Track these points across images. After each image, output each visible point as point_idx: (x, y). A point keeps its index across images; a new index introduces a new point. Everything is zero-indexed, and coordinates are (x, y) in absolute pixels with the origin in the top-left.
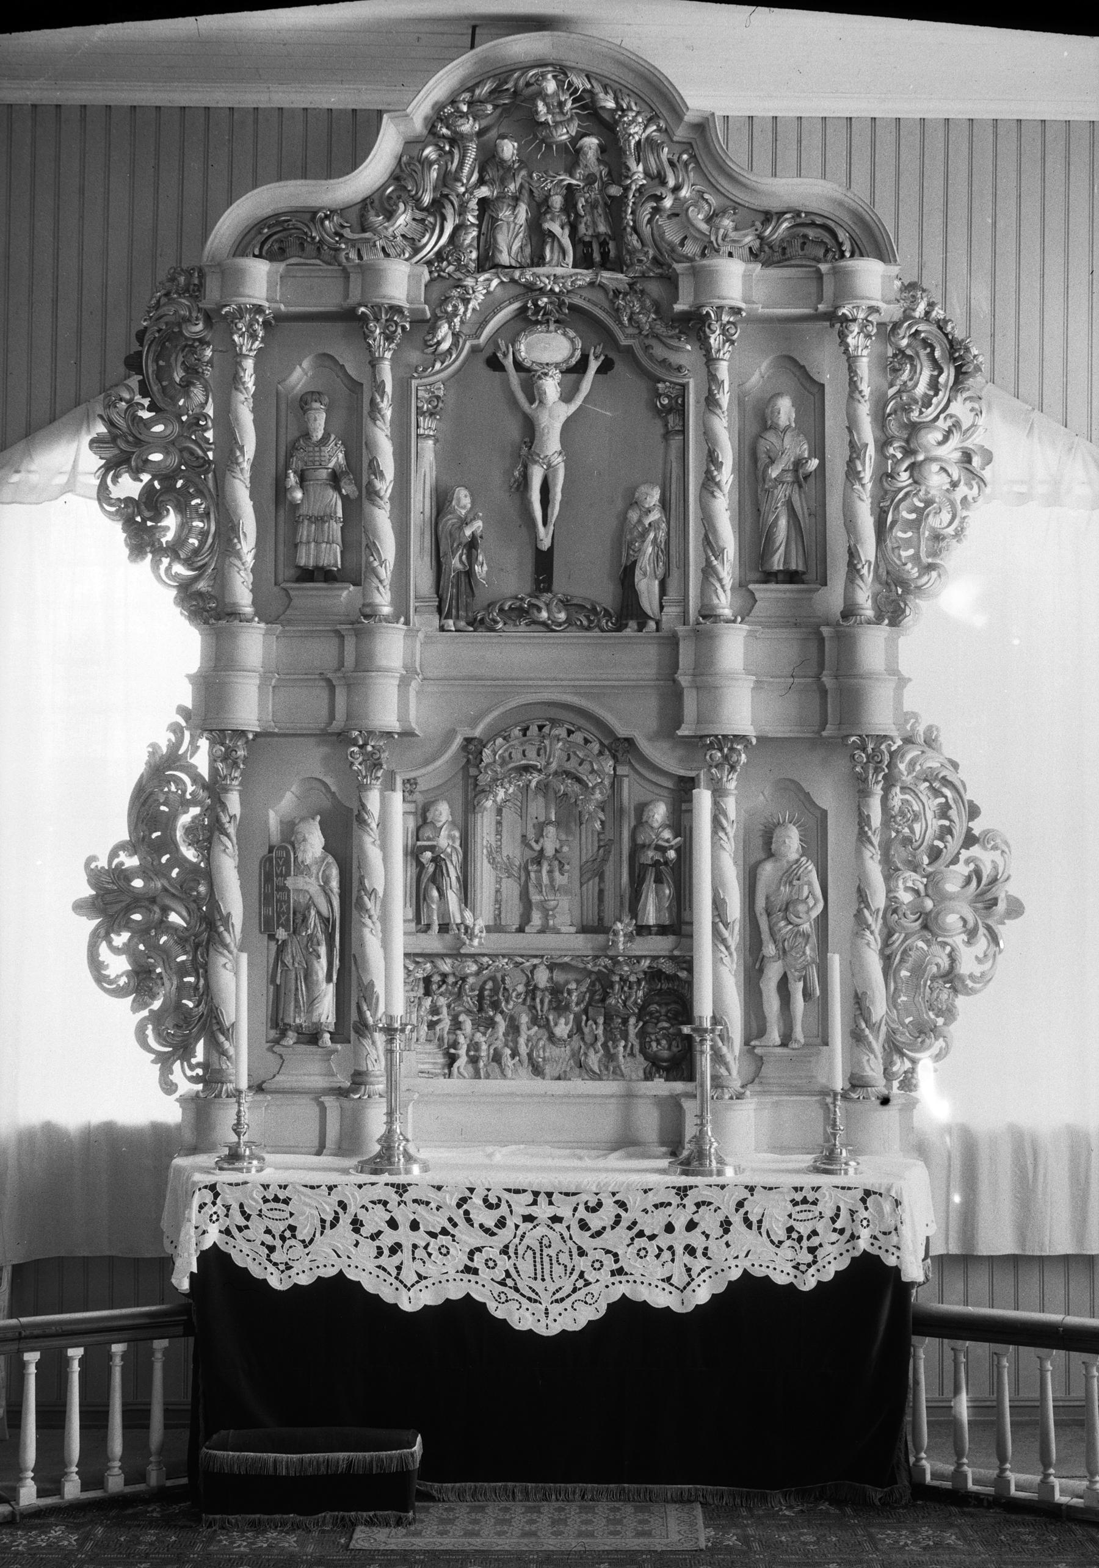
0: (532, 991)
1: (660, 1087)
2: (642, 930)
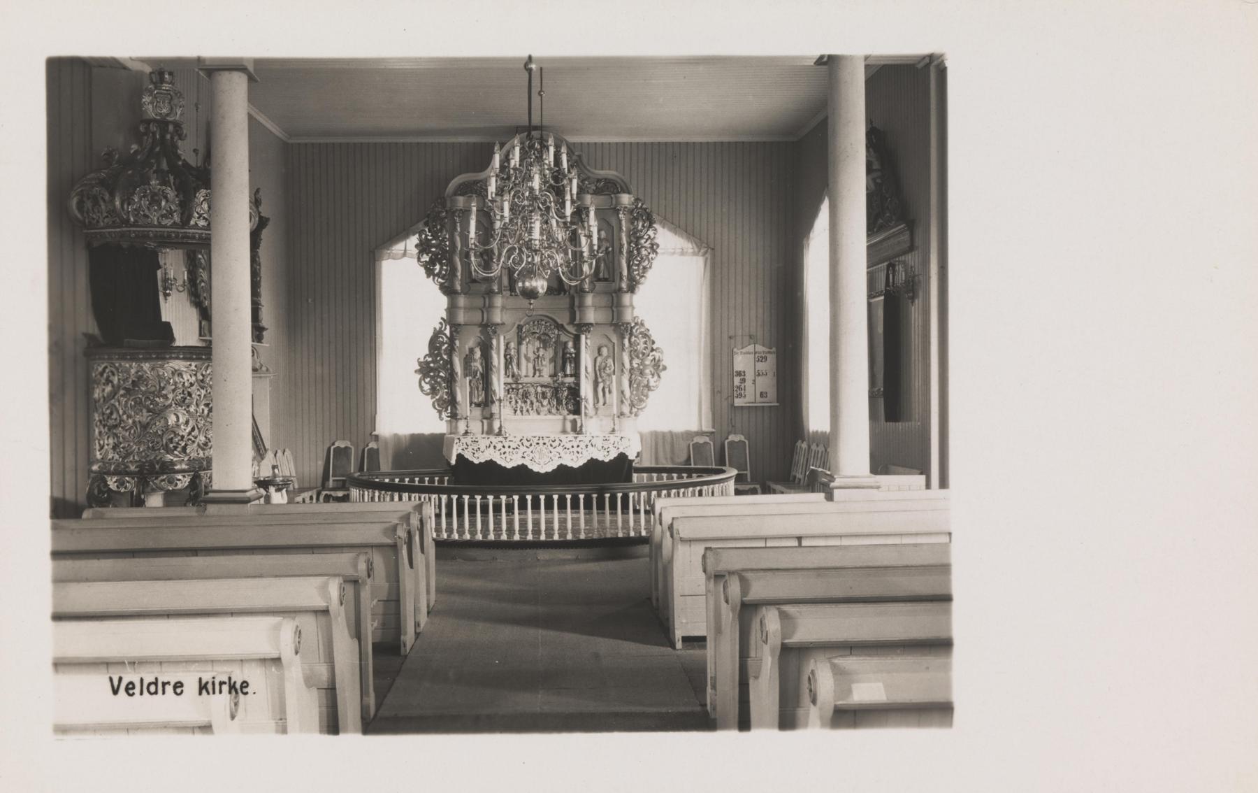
0: (537, 393)
1: (571, 417)
2: (566, 376)
